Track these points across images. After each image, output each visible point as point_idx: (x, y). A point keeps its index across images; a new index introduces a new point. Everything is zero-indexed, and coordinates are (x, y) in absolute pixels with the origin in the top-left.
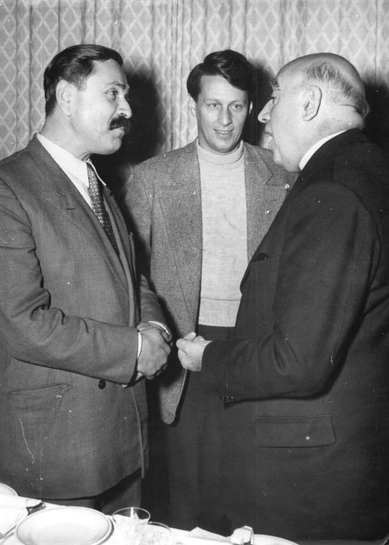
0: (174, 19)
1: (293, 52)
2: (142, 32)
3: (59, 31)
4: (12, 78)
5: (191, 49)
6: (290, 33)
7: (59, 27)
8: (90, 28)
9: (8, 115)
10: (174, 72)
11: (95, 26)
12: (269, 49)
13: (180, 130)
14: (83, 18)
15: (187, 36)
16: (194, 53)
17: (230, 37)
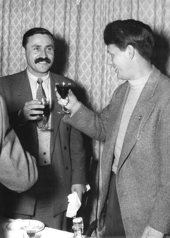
0: (104, 12)
1: (160, 15)
2: (85, 73)
3: (55, 7)
4: (32, 17)
5: (113, 14)
6: (158, 6)
7: (55, 5)
8: (67, 29)
9: (30, 24)
10: (103, 50)
11: (71, 4)
12: (149, 14)
13: (107, 77)
14: (65, 12)
15: (112, 9)
16: (115, 16)
17: (132, 8)
